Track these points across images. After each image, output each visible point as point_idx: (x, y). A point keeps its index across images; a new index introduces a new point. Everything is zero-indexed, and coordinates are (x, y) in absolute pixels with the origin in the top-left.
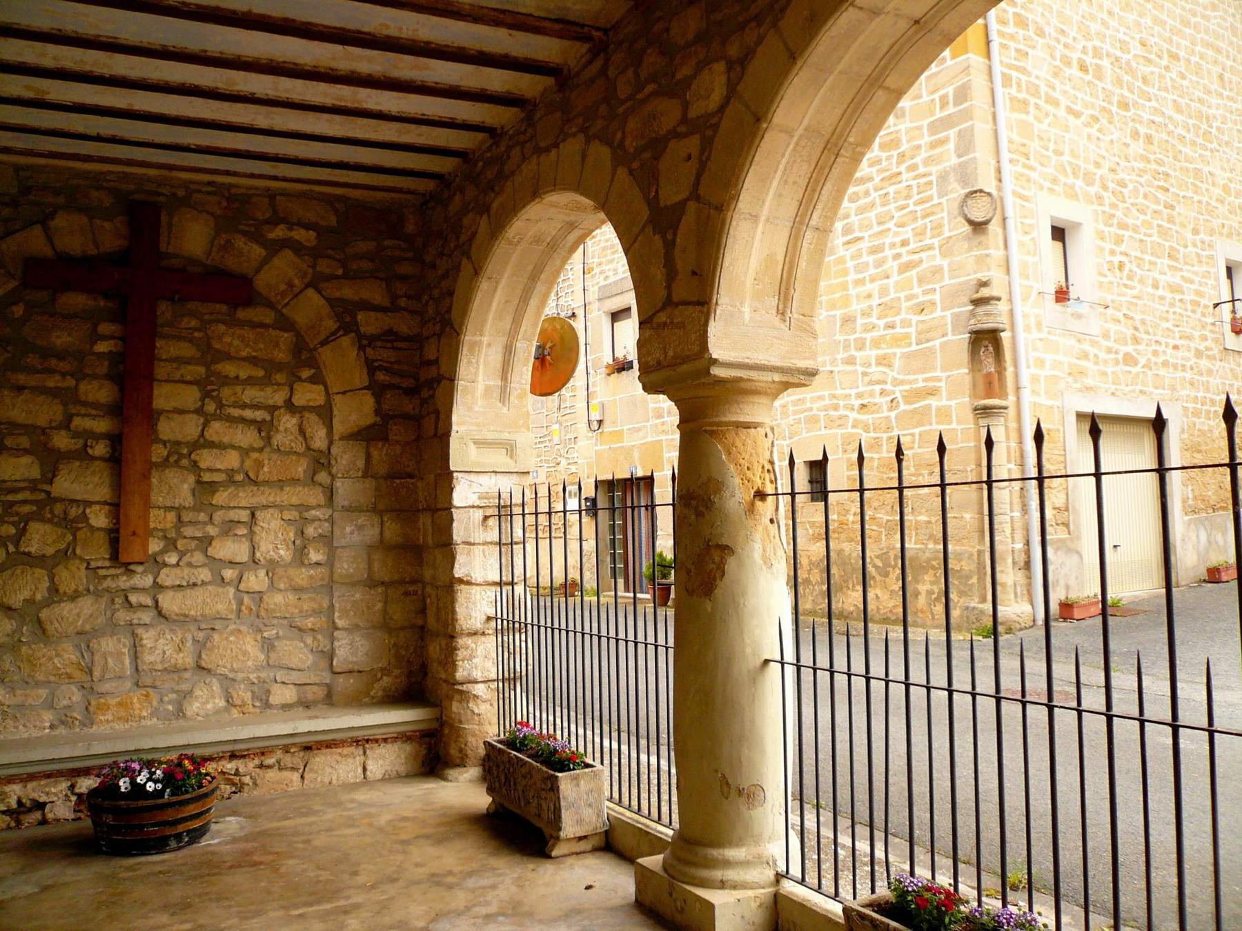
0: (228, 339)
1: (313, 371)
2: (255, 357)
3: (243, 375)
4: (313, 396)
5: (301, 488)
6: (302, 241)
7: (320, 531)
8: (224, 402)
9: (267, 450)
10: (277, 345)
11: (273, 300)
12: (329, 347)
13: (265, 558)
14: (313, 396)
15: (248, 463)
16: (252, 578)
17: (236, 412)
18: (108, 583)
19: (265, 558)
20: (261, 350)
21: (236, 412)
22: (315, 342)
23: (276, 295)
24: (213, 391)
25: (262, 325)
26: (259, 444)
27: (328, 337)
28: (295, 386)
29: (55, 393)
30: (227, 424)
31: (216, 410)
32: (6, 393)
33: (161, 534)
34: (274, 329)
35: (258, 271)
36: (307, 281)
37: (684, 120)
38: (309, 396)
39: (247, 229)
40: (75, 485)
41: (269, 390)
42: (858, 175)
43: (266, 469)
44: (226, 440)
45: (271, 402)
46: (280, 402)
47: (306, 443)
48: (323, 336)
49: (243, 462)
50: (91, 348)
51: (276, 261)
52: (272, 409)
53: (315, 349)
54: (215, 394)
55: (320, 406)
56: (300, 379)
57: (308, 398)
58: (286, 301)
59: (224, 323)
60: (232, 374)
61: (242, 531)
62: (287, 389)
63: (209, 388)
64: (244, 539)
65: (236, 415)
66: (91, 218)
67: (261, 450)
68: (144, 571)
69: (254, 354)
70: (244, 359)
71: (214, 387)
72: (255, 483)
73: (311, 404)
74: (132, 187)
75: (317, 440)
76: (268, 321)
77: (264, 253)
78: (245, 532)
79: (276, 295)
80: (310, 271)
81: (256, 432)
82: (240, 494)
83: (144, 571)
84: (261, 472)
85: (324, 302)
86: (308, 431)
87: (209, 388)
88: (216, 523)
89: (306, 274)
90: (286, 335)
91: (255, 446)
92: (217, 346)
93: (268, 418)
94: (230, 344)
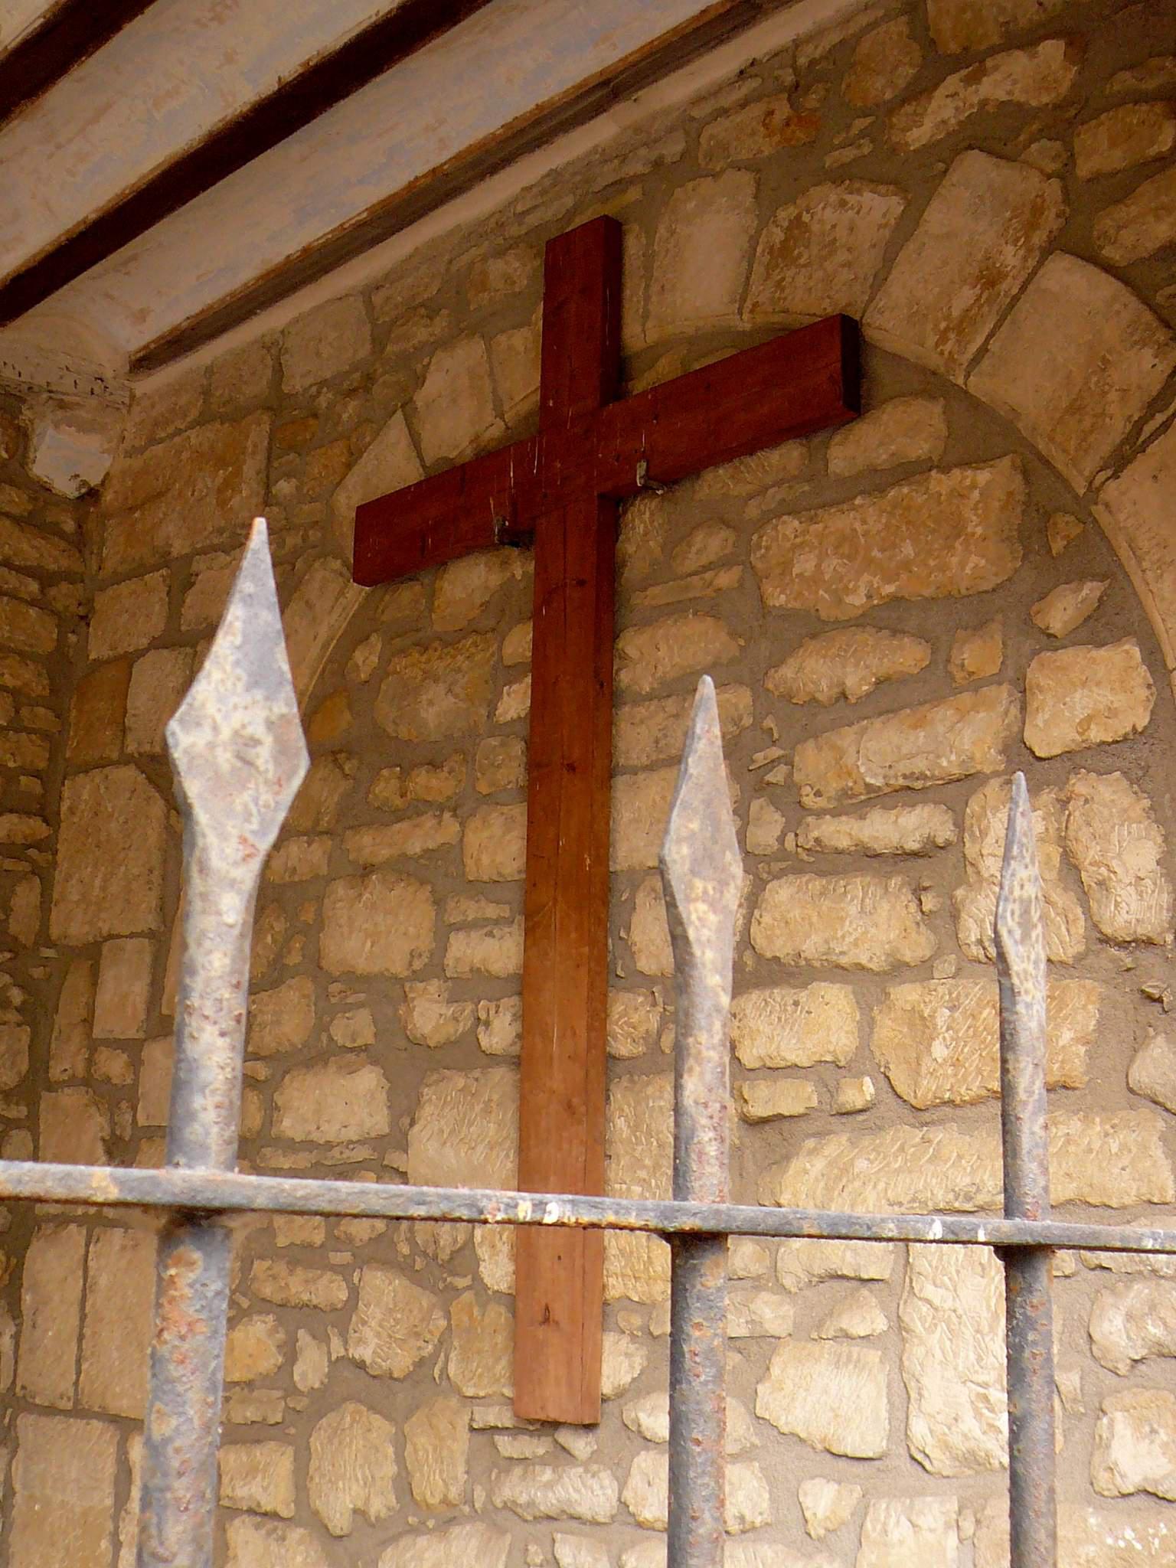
0: (805, 564)
1: (1091, 590)
2: (896, 600)
3: (857, 681)
4: (1103, 697)
5: (1075, 1125)
6: (1019, 96)
7: (1155, 1331)
8: (809, 800)
9: (947, 965)
10: (958, 529)
11: (935, 361)
12: (1140, 467)
13: (946, 1447)
14: (1103, 697)
15: (888, 1029)
16: (900, 1531)
17: (839, 832)
18: (515, 1489)
19: (946, 1447)
20: (906, 565)
21: (839, 832)
22: (1090, 464)
23: (943, 338)
24: (773, 763)
25: (909, 471)
26: (917, 947)
27: (1139, 426)
28: (1035, 675)
29: (404, 868)
30: (818, 884)
31: (781, 840)
32: (341, 892)
33: (637, 1321)
34: (945, 469)
35: (880, 280)
36: (1039, 238)
37: (349, 438)
38: (1082, 703)
39: (849, 154)
40: (448, 1151)
41: (943, 715)
42: (539, 392)
43: (939, 1050)
44: (812, 946)
45: (949, 763)
46: (989, 758)
47: (1087, 912)
48: (1117, 428)
49: (867, 1027)
50: (491, 715)
51: (936, 217)
52: (968, 781)
53: (1094, 491)
54: (777, 776)
55: (1135, 736)
56: (1051, 641)
57: (1081, 714)
58: (973, 348)
59: (793, 512)
60: (825, 690)
61: (867, 1319)
62: (1003, 693)
63: (760, 757)
64: (873, 1356)
65: (844, 843)
66: (489, 340)
67: (923, 970)
68: (595, 1457)
69: (890, 589)
70: (862, 621)
71: (776, 752)
72: (918, 1113)
73: (1096, 734)
74: (569, 201)
75: (1126, 894)
76: (920, 448)
77: (894, 205)
78: (881, 1324)
79: (943, 338)
80: (1054, 188)
81: (907, 896)
82: (861, 1164)
83: (595, 1457)
84: (927, 1064)
85: (1109, 286)
86: (1089, 853)
87: (760, 757)
88: (788, 1282)
89: (1037, 210)
90: (983, 476)
91: (908, 956)
92: (778, 599)
93: (945, 832)
94: (815, 580)
